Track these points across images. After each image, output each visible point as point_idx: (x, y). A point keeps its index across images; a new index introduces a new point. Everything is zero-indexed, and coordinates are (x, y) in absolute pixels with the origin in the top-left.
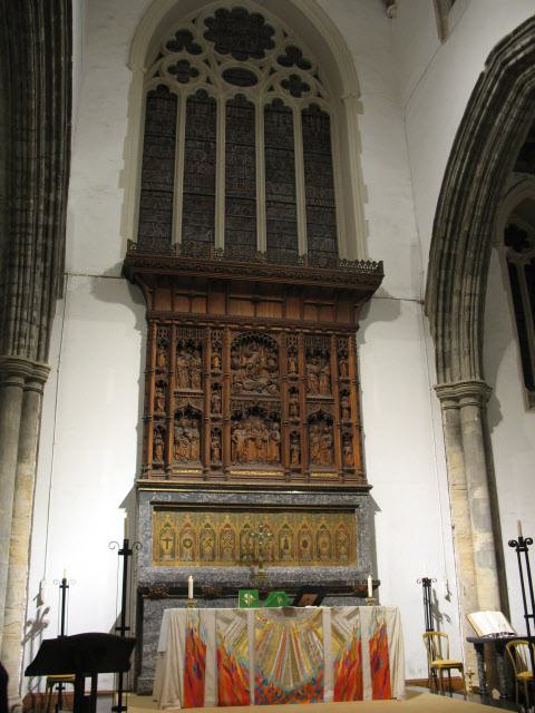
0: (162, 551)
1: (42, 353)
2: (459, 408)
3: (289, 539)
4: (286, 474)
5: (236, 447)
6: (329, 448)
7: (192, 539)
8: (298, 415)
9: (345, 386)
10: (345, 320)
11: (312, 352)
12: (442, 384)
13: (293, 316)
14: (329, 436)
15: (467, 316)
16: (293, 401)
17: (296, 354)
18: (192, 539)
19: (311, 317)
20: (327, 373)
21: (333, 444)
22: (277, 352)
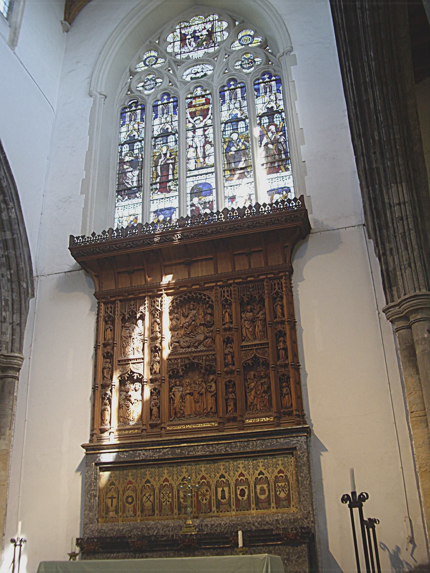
0: (108, 507)
1: (17, 345)
2: (409, 327)
3: (226, 489)
4: (219, 423)
5: (174, 403)
6: (265, 392)
7: (133, 495)
8: (233, 364)
9: (280, 327)
10: (276, 260)
11: (246, 300)
12: (391, 304)
13: (224, 268)
14: (266, 380)
15: (400, 227)
16: (227, 351)
17: (230, 305)
18: (133, 495)
19: (242, 265)
20: (261, 317)
21: (269, 387)
22: (211, 307)
